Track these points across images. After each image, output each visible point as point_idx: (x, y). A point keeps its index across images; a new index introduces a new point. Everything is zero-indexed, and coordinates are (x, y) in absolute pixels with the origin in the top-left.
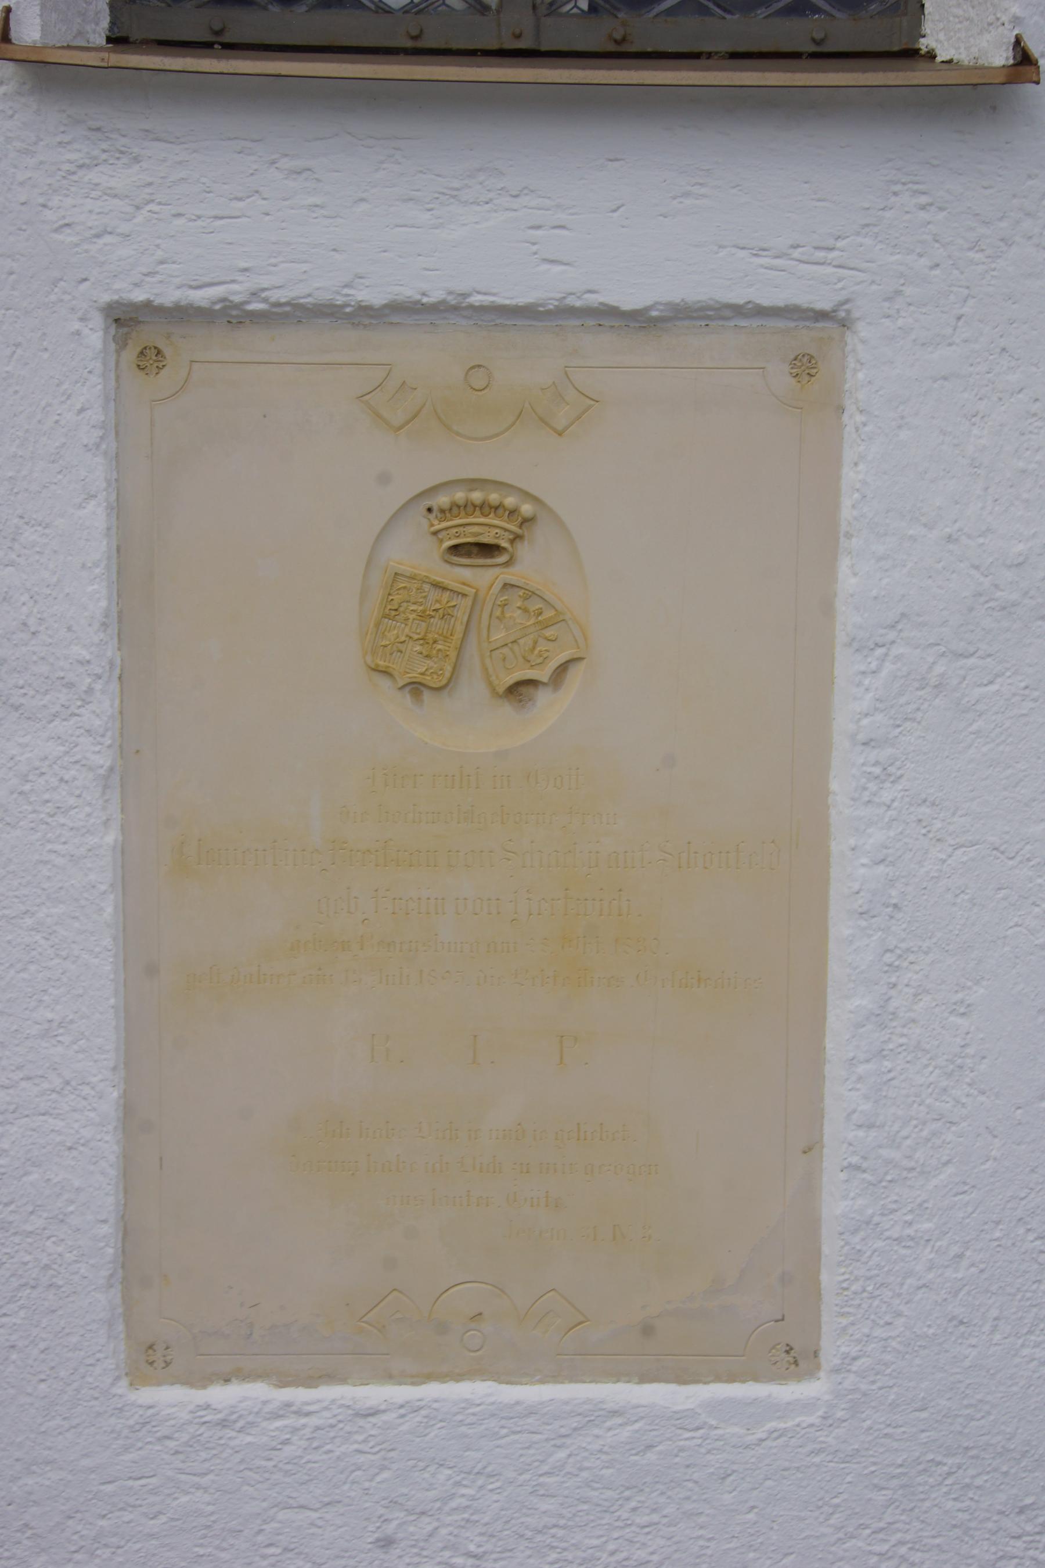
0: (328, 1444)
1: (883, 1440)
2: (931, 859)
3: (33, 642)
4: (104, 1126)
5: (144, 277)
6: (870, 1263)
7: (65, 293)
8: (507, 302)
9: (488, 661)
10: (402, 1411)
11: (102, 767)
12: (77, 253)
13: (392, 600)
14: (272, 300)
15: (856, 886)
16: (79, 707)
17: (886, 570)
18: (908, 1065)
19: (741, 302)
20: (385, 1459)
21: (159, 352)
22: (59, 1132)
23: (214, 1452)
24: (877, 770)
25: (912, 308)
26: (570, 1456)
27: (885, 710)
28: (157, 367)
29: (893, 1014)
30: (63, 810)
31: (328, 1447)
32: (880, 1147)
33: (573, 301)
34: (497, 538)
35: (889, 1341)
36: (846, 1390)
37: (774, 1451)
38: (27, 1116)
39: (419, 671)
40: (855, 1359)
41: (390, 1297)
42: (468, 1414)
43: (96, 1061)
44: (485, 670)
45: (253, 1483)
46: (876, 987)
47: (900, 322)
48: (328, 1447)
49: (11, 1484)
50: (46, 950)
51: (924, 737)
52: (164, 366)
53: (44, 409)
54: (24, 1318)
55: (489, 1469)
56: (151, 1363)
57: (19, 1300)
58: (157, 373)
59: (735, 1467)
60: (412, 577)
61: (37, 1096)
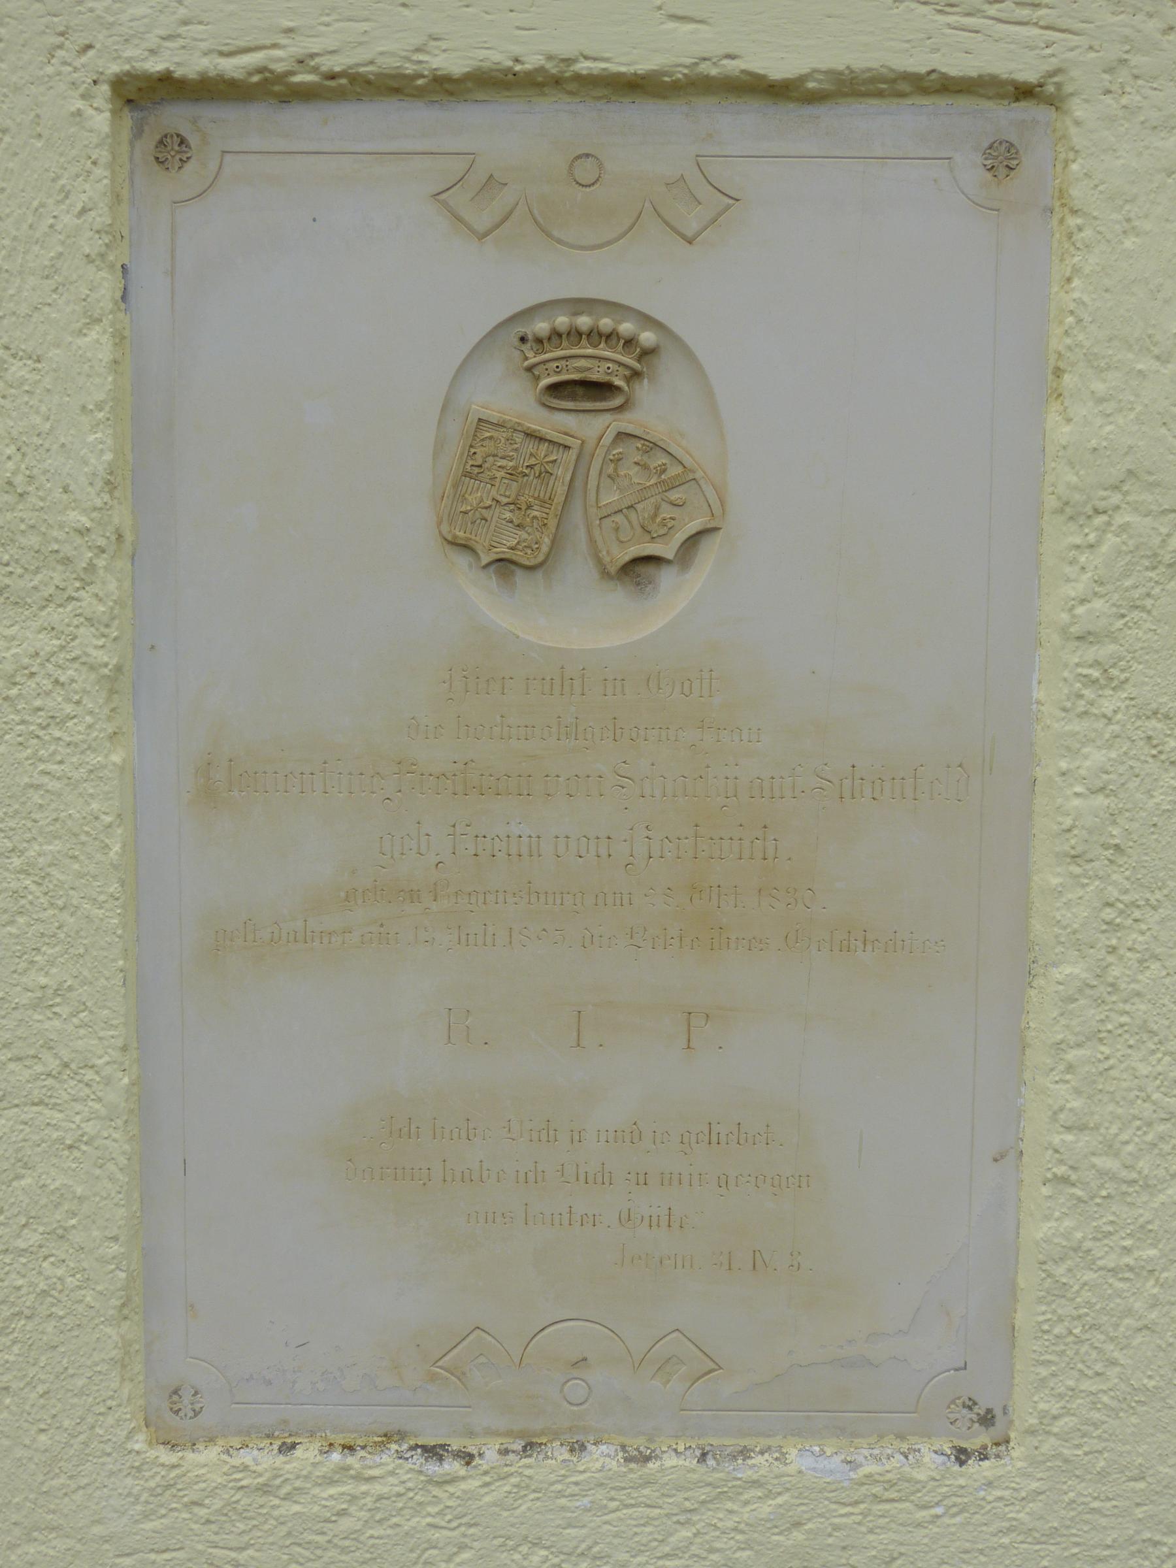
0: (395, 1516)
1: (1088, 1516)
2: (1162, 787)
3: (20, 507)
4: (112, 1120)
5: (161, 41)
6: (1079, 1300)
7: (65, 63)
8: (623, 69)
9: (596, 533)
10: (487, 1479)
11: (106, 665)
12: (80, 13)
13: (475, 453)
14: (324, 69)
15: (1068, 822)
16: (78, 589)
17: (1109, 415)
18: (1129, 1051)
19: (923, 70)
20: (464, 1535)
21: (183, 142)
22: (56, 1127)
23: (255, 1522)
24: (1095, 673)
25: (1140, 82)
26: (695, 1535)
27: (1106, 595)
28: (181, 160)
29: (1112, 985)
30: (58, 720)
31: (395, 1520)
32: (1094, 1154)
33: (707, 69)
34: (609, 374)
35: (1100, 1396)
36: (1043, 1455)
37: (953, 1529)
38: (17, 1106)
39: (508, 544)
40: (1055, 1418)
41: (471, 1337)
42: (570, 1483)
43: (100, 1039)
44: (592, 541)
45: (301, 1560)
46: (1092, 950)
47: (1124, 101)
48: (395, 1520)
49: (8, 1552)
50: (38, 898)
51: (1155, 630)
52: (188, 158)
53: (37, 210)
54: (19, 1355)
55: (596, 1549)
56: (177, 1412)
57: (11, 1332)
58: (180, 168)
59: (903, 1550)
60: (500, 425)
61: (28, 1081)
